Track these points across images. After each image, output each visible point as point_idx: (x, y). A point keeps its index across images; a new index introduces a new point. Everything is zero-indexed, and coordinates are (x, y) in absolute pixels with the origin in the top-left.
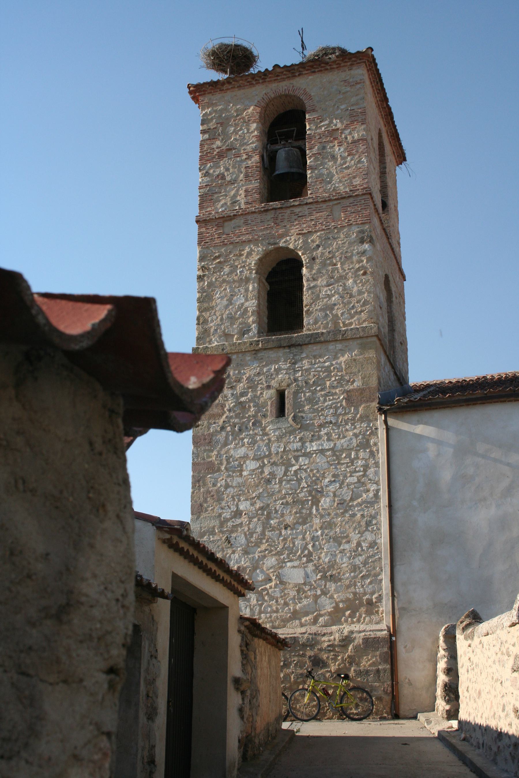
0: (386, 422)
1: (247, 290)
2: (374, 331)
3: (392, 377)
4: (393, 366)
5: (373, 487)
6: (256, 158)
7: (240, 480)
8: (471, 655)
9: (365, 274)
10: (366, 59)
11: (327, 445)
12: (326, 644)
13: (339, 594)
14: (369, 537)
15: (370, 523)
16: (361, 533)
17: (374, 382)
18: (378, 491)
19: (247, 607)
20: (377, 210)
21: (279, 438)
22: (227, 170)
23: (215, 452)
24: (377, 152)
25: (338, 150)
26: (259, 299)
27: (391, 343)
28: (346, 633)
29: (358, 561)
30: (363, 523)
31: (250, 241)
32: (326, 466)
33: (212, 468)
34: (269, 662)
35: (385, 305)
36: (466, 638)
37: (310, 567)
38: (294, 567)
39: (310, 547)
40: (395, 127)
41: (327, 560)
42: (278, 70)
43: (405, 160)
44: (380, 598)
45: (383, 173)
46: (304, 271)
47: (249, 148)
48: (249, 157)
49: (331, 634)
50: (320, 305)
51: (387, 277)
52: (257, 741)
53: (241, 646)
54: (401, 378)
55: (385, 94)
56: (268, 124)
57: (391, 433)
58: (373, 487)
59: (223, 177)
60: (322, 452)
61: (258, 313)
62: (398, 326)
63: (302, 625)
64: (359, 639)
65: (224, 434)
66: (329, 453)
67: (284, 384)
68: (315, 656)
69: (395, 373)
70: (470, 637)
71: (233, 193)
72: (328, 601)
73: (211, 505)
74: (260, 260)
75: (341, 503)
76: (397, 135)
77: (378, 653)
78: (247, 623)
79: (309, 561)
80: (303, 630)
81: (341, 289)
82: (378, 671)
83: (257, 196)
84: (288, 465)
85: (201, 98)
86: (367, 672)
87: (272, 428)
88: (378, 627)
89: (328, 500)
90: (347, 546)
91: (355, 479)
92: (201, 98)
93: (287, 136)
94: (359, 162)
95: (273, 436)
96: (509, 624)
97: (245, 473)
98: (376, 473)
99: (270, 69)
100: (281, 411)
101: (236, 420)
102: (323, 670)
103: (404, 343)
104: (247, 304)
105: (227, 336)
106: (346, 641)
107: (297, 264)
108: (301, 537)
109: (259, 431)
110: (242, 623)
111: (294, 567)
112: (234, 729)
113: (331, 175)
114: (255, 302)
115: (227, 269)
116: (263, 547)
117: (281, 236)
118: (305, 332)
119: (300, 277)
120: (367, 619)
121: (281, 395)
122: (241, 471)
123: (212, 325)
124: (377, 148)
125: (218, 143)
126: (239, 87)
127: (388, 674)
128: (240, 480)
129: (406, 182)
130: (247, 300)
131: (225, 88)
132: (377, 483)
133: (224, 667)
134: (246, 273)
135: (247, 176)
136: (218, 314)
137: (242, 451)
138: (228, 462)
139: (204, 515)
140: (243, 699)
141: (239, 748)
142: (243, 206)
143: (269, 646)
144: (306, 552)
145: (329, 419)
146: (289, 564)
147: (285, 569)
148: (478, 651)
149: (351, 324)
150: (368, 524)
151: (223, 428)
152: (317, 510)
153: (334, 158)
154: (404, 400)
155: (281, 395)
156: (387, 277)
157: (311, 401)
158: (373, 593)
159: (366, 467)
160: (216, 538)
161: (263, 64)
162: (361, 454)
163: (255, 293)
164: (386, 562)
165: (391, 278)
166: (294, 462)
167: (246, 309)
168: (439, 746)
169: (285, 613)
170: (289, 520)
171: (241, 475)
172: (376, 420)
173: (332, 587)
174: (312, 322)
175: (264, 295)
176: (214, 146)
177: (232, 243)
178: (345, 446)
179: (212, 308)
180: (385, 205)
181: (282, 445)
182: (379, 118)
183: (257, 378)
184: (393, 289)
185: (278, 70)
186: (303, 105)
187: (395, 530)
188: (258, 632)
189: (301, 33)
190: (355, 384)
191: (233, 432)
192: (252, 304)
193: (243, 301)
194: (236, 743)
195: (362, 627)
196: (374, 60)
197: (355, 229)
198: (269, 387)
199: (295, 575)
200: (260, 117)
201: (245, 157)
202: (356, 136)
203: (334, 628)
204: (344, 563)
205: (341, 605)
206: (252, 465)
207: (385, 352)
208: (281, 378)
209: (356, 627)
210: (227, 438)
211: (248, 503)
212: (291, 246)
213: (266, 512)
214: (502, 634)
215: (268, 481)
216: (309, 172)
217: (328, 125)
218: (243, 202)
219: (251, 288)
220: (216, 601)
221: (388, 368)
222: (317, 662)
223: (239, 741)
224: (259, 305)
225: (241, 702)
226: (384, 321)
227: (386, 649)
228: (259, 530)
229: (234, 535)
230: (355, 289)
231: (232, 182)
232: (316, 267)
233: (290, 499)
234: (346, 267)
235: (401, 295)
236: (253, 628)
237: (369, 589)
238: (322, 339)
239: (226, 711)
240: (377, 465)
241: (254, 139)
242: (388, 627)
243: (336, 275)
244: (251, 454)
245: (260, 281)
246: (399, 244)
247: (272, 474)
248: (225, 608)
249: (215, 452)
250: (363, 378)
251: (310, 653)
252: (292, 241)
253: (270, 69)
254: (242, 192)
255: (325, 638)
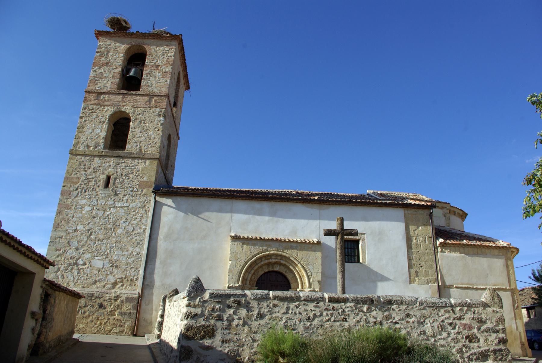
0: (155, 198)
1: (102, 127)
2: (158, 156)
3: (164, 179)
4: (165, 175)
5: (144, 227)
6: (119, 70)
7: (80, 215)
8: (169, 310)
9: (158, 130)
10: (178, 39)
11: (125, 205)
12: (107, 298)
13: (118, 274)
14: (138, 250)
15: (139, 243)
16: (134, 248)
17: (153, 179)
18: (145, 229)
19: (50, 274)
20: (170, 104)
21: (103, 198)
22: (105, 71)
23: (71, 200)
24: (176, 80)
25: (158, 74)
26: (107, 132)
27: (166, 163)
28: (118, 293)
29: (130, 260)
30: (136, 243)
31: (108, 106)
32: (123, 214)
33: (68, 207)
34: (67, 304)
35: (166, 147)
36: (169, 302)
37: (107, 261)
38: (99, 260)
39: (108, 251)
40: (187, 73)
41: (115, 258)
42: (138, 34)
43: (189, 88)
44: (137, 279)
45: (177, 90)
46: (131, 124)
47: (117, 64)
48: (116, 68)
49: (111, 293)
50: (135, 140)
51: (170, 135)
52: (47, 345)
53: (41, 295)
54: (169, 182)
55: (184, 57)
56: (129, 56)
57: (157, 204)
58: (144, 227)
59: (102, 75)
60: (122, 207)
61: (105, 138)
62: (171, 158)
63: (97, 288)
64: (123, 297)
65: (77, 192)
66: (126, 208)
67: (111, 173)
68: (101, 303)
69: (165, 178)
70: (170, 302)
71: (105, 82)
72: (112, 277)
73: (63, 225)
74: (112, 115)
75: (127, 232)
76: (187, 77)
77: (132, 304)
78: (47, 283)
79: (107, 257)
80: (98, 290)
81: (146, 135)
82: (130, 313)
83: (116, 86)
84: (105, 211)
85: (100, 37)
86: (125, 313)
87: (102, 193)
88: (134, 292)
89: (121, 230)
90: (126, 253)
91: (135, 222)
92: (100, 37)
93: (136, 65)
94: (166, 81)
95: (101, 196)
96: (182, 297)
97: (83, 212)
98: (146, 221)
99: (135, 32)
100: (107, 185)
101: (84, 187)
102: (104, 310)
103: (173, 167)
104: (101, 134)
105: (88, 147)
106: (117, 298)
107: (128, 120)
108: (104, 245)
109: (94, 192)
110: (44, 283)
111: (99, 260)
112: (26, 339)
113: (152, 85)
114: (105, 133)
115: (95, 116)
116: (86, 248)
117: (124, 106)
118: (126, 151)
119: (129, 126)
120: (130, 288)
121: (109, 178)
122: (82, 210)
123: (82, 140)
124: (176, 79)
125: (103, 59)
126: (119, 37)
127: (135, 315)
128: (80, 215)
129: (187, 99)
130: (101, 131)
131: (112, 35)
132: (146, 225)
133: (26, 305)
134: (103, 119)
135: (113, 76)
136: (86, 135)
137: (84, 201)
138: (76, 206)
139: (59, 229)
140: (36, 323)
141: (28, 350)
142: (109, 89)
143: (69, 296)
144: (106, 253)
145: (128, 193)
146: (96, 258)
147: (95, 261)
148: (172, 308)
149: (147, 151)
150: (138, 243)
151: (77, 189)
152: (115, 234)
153: (155, 77)
154: (164, 188)
155: (109, 178)
156: (170, 135)
157: (121, 183)
158: (134, 276)
159: (142, 217)
160: (63, 240)
161: (133, 30)
162: (141, 211)
163: (106, 129)
164: (143, 262)
165: (172, 136)
166: (108, 210)
167: (100, 136)
168: (147, 352)
169: (91, 281)
170: (101, 237)
171: (81, 212)
172: (151, 196)
173: (115, 271)
174: (131, 147)
175: (111, 132)
176: (101, 60)
177: (100, 105)
178: (134, 206)
179: (84, 132)
180: (175, 104)
181: (104, 202)
182: (180, 66)
183: (99, 169)
184: (172, 141)
185: (138, 34)
186: (146, 52)
187: (150, 248)
188: (57, 289)
189: (154, 23)
190: (144, 179)
191: (81, 191)
192: (103, 134)
193: (99, 131)
194: (27, 347)
195: (127, 292)
196: (182, 40)
197: (158, 110)
198: (103, 173)
199: (98, 263)
200: (126, 52)
201: (114, 67)
202: (167, 70)
203: (113, 291)
204: (123, 260)
205: (118, 280)
206: (88, 209)
207: (162, 167)
208: (110, 171)
209: (123, 291)
210: (78, 194)
211: (82, 226)
212: (127, 112)
213: (90, 232)
214: (180, 301)
215: (94, 217)
216: (142, 81)
217: (155, 63)
218: (109, 87)
219: (104, 127)
220: (26, 269)
221: (162, 175)
222: (101, 306)
223: (29, 346)
224: (106, 135)
225: (34, 325)
226: (164, 153)
227: (136, 303)
228: (85, 240)
229: (72, 241)
230: (153, 136)
231: (105, 77)
232: (136, 123)
233: (103, 227)
234: (151, 125)
235: (176, 146)
236: (52, 287)
237: (133, 274)
238: (133, 156)
239: (22, 330)
240: (147, 217)
241: (121, 61)
242: (139, 293)
243: (145, 128)
244: (88, 203)
245: (109, 125)
246: (179, 123)
247: (97, 214)
248: (34, 274)
249: (71, 200)
250: (148, 177)
251: (98, 301)
252: (128, 109)
253: (135, 32)
254: (110, 83)
255: (108, 295)
